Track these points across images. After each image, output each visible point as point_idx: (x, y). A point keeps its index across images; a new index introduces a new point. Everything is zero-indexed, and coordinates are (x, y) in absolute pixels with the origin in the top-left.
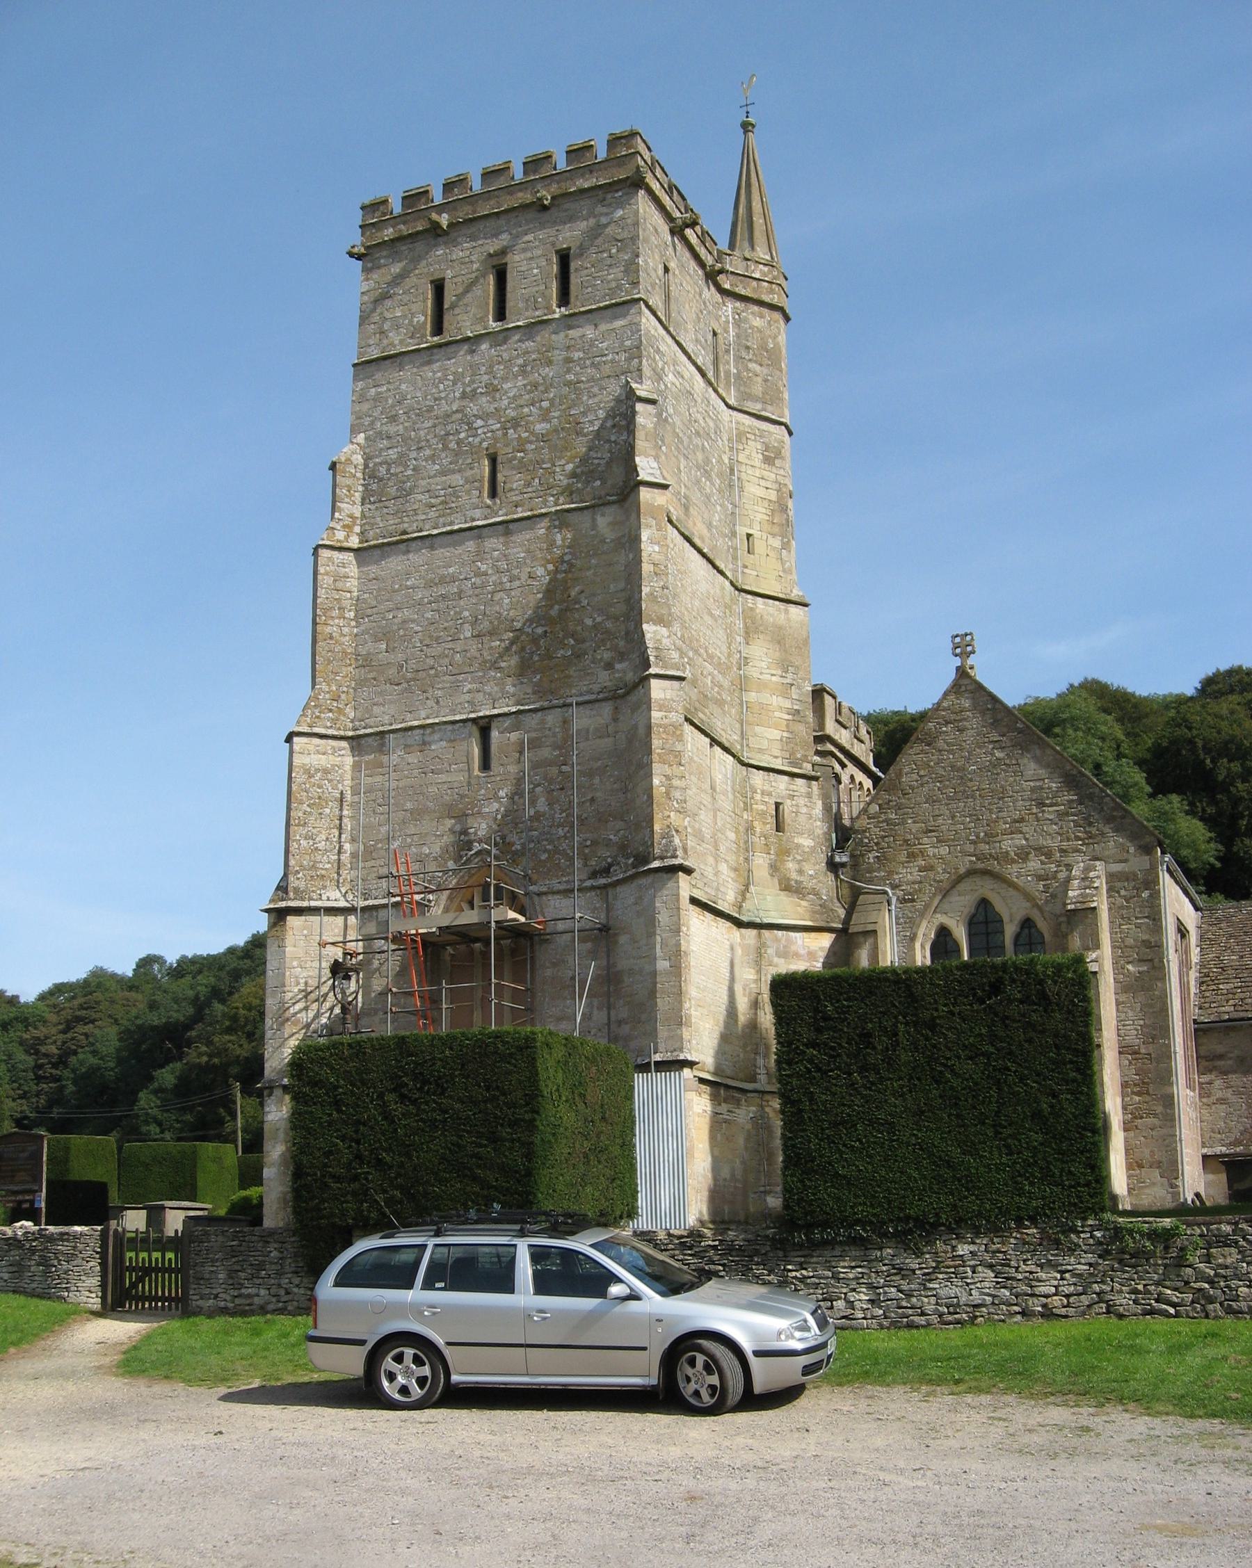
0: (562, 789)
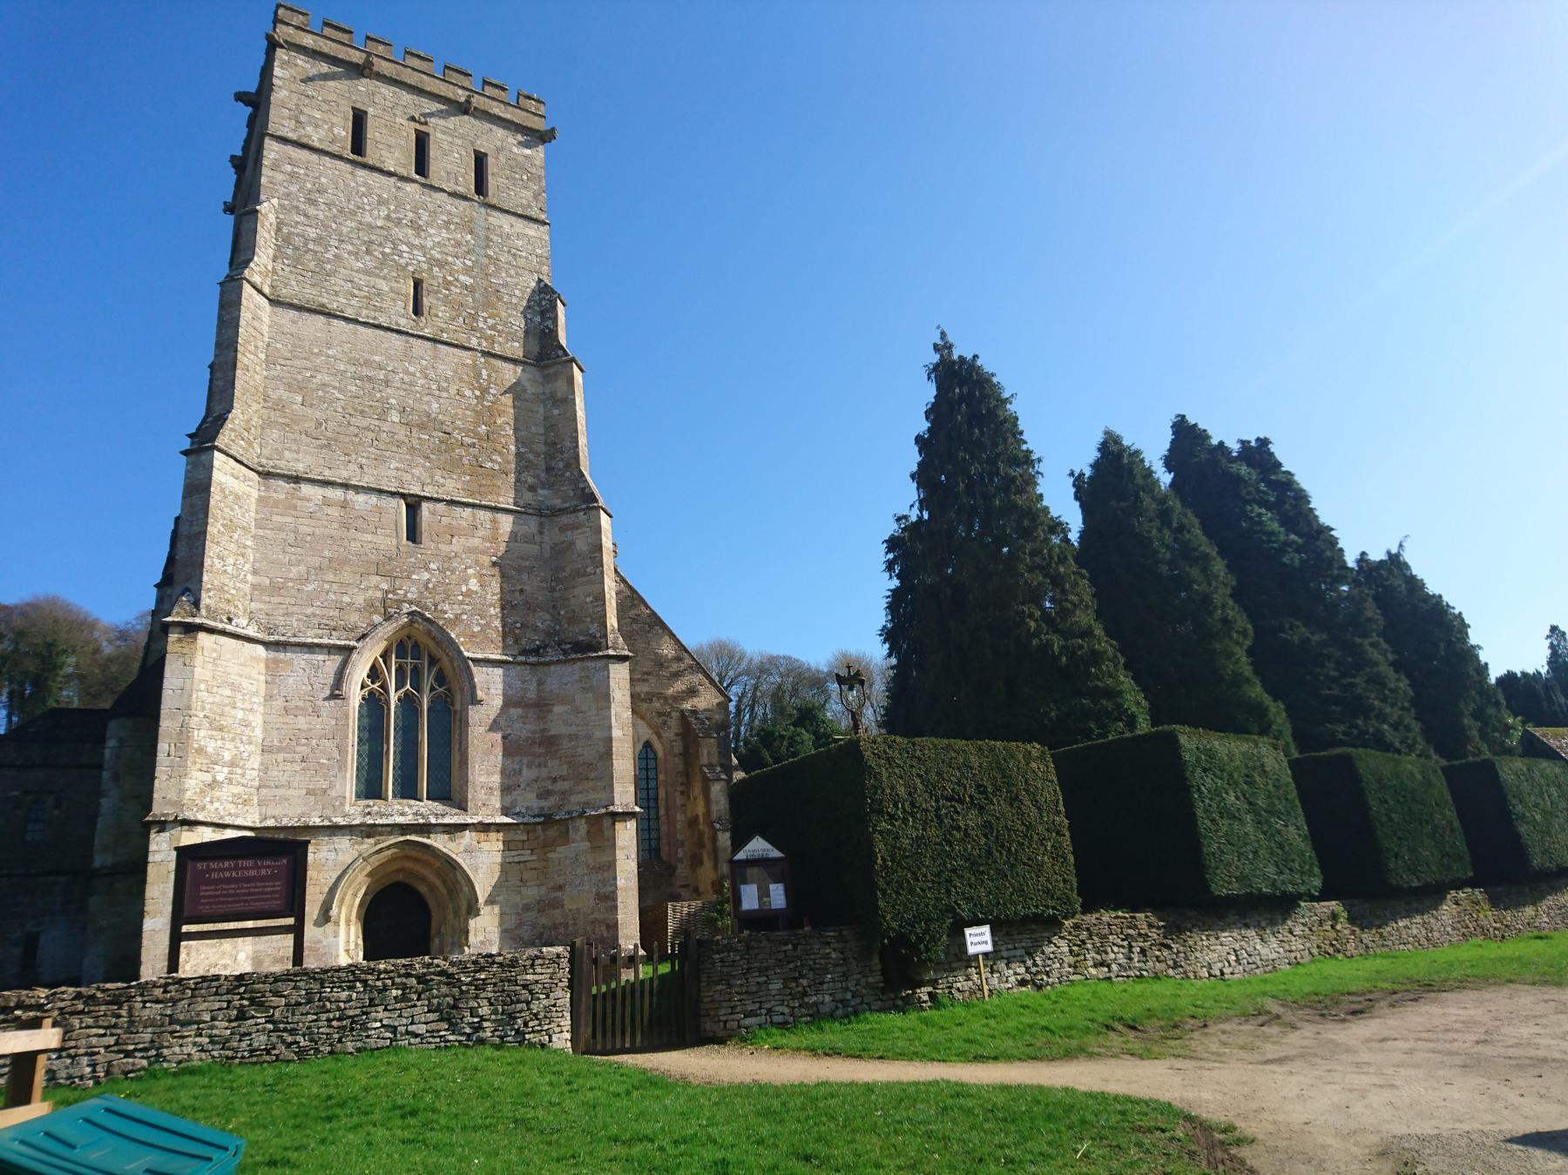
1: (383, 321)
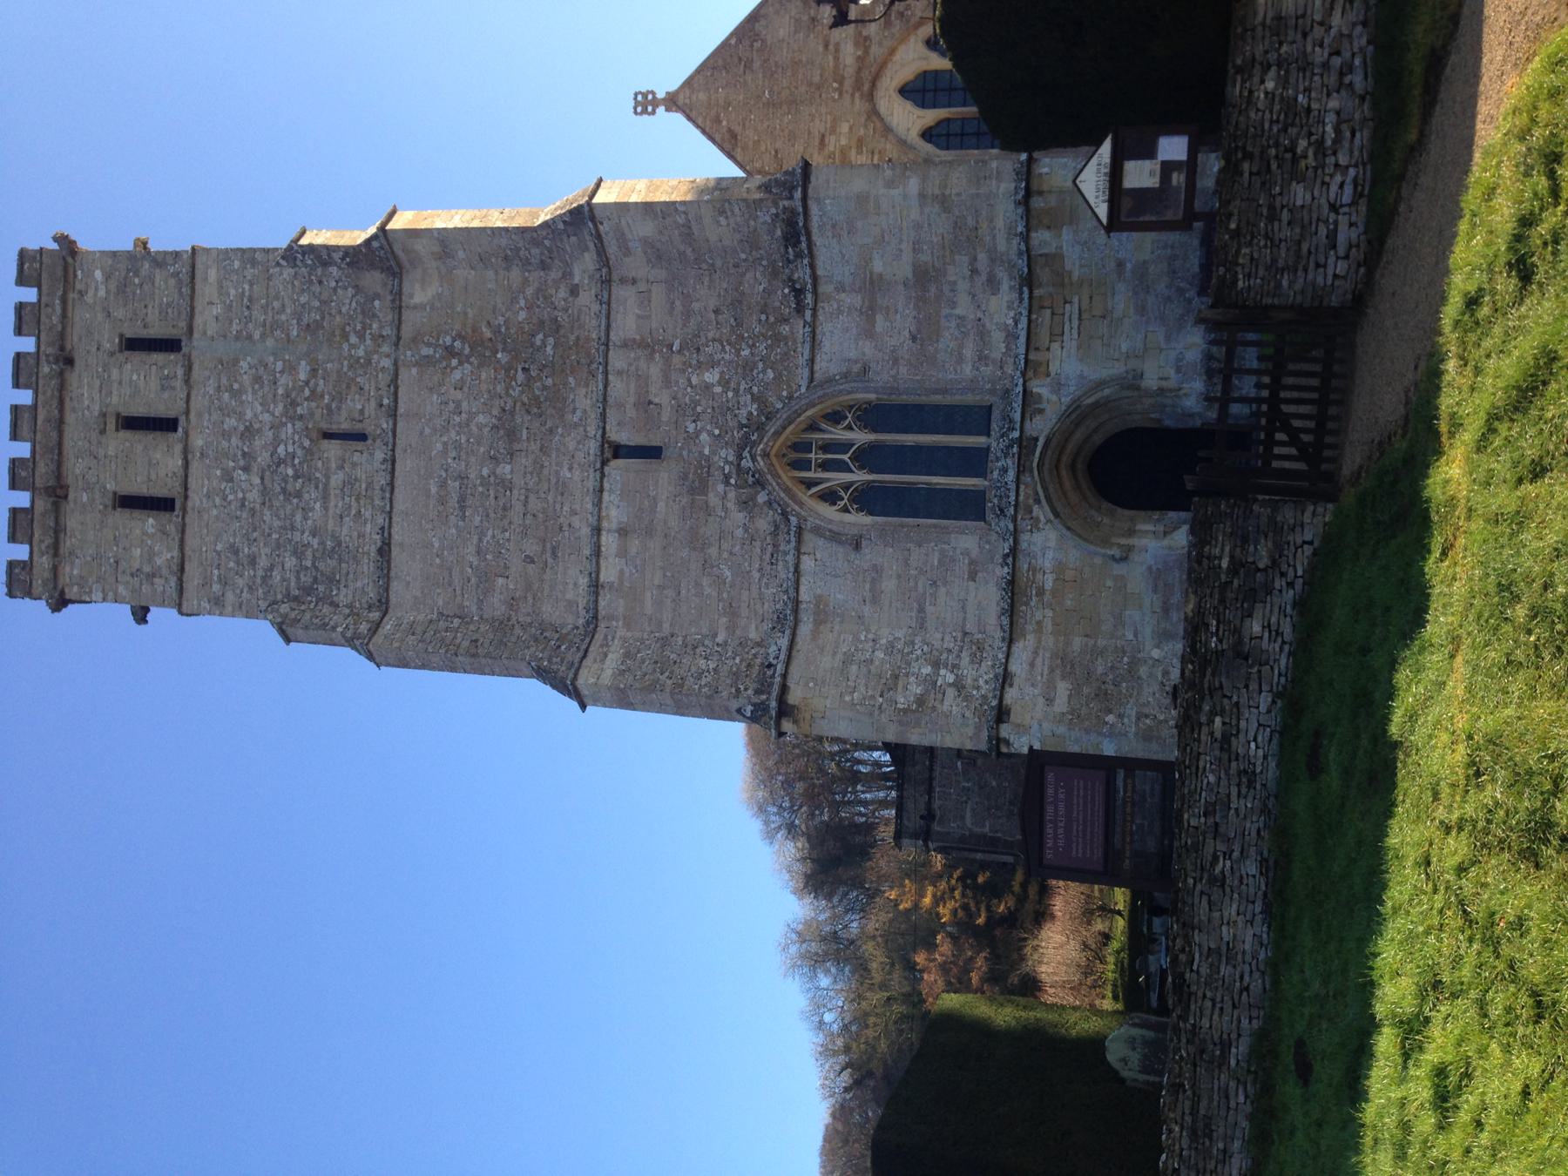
0: (698, 350)
1: (382, 480)
